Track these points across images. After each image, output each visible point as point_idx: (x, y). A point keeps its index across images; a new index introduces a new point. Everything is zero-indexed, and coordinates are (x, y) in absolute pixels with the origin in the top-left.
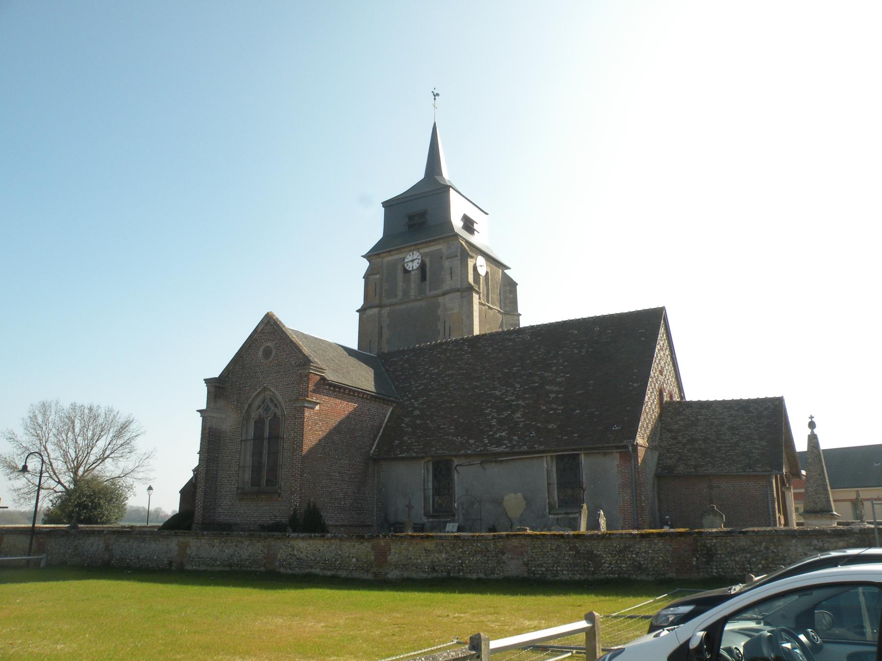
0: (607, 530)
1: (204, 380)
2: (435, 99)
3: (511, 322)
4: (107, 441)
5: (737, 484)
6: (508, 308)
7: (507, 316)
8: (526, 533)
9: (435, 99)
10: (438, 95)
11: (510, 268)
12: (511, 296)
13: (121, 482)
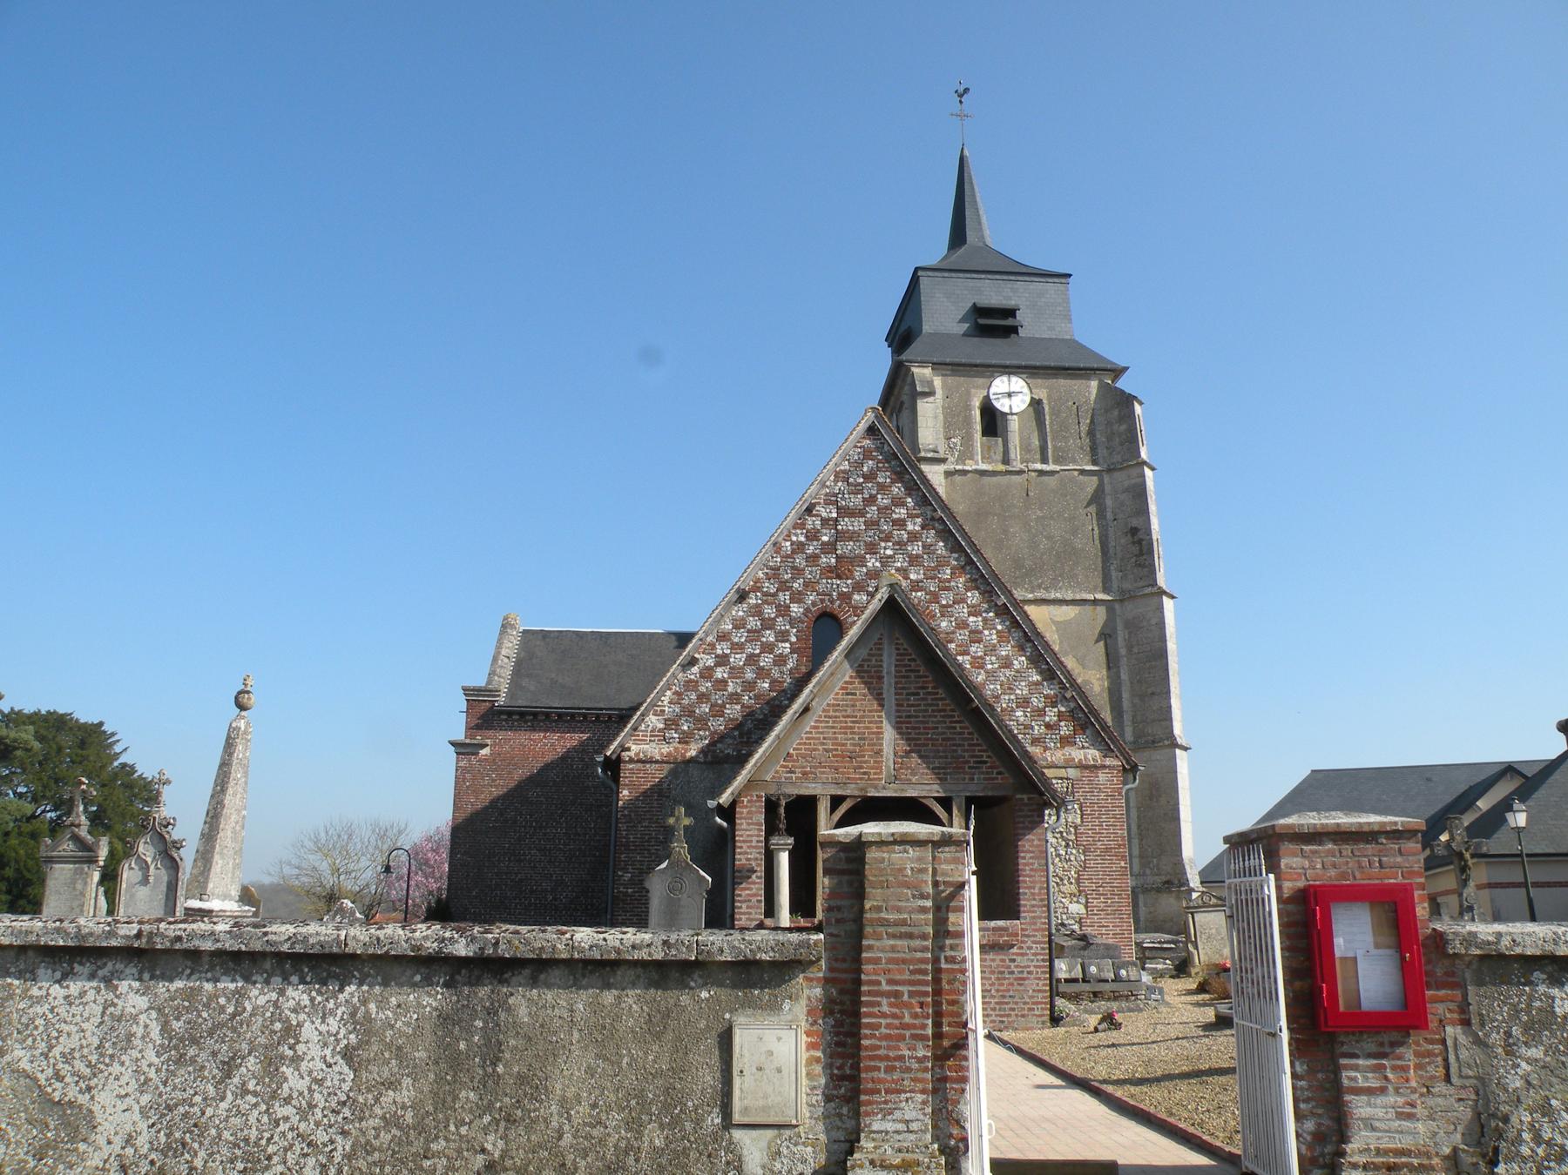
0: (1341, 958)
1: (465, 689)
2: (961, 102)
3: (1126, 484)
4: (1183, 1090)
5: (993, 960)
6: (1119, 456)
7: (1117, 475)
8: (881, 988)
9: (961, 102)
10: (966, 90)
11: (1127, 368)
12: (1123, 427)
13: (237, 898)
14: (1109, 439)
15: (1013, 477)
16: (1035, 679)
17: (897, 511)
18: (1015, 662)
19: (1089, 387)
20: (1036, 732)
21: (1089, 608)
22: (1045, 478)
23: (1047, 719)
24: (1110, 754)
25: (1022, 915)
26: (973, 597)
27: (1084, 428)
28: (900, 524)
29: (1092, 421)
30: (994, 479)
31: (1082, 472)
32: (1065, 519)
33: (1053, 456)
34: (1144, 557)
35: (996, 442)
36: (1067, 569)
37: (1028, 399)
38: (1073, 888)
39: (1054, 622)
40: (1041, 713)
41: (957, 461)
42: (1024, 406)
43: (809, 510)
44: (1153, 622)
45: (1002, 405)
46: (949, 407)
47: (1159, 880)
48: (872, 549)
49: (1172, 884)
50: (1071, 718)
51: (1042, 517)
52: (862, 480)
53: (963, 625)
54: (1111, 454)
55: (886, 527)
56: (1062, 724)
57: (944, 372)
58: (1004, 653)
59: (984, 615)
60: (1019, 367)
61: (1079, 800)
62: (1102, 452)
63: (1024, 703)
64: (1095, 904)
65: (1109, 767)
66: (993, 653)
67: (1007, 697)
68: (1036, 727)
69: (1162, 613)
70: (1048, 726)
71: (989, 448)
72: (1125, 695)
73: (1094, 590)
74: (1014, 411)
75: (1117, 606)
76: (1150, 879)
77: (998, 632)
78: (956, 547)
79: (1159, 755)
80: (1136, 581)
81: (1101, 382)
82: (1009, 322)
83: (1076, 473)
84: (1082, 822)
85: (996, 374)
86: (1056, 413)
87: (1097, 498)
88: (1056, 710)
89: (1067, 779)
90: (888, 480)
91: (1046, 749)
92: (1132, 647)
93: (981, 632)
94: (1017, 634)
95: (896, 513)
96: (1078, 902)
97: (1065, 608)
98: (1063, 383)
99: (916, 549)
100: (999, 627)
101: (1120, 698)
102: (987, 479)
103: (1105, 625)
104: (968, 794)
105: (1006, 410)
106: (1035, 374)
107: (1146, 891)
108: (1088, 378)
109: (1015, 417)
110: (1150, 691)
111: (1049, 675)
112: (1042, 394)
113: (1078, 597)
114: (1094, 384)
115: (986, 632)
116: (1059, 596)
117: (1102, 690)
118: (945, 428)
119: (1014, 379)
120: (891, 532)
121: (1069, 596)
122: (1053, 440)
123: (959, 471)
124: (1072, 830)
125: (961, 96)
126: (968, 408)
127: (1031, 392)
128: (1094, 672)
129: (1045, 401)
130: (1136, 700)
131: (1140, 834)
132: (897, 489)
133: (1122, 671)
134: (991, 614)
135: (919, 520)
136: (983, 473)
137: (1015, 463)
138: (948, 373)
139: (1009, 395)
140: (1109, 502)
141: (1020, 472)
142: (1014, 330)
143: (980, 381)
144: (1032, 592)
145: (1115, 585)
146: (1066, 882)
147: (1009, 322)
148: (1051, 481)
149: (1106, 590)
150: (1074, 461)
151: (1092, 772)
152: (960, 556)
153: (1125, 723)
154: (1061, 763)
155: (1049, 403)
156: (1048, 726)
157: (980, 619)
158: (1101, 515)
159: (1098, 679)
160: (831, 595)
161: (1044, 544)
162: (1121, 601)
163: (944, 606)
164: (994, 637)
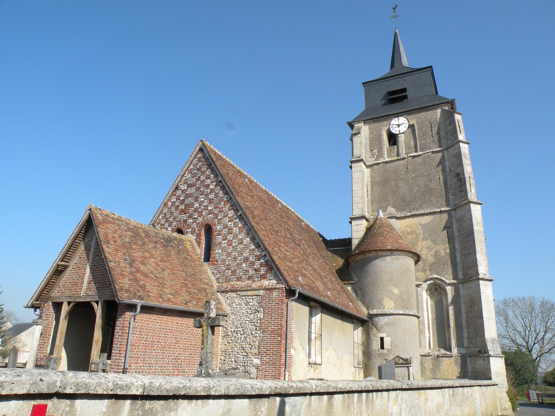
3: (454, 153)
9: (395, 11)
14: (447, 134)
15: (400, 161)
16: (252, 248)
17: (207, 181)
18: (245, 241)
19: (436, 113)
20: (250, 273)
21: (438, 216)
22: (415, 159)
23: (255, 267)
24: (280, 282)
25: (112, 357)
26: (231, 213)
27: (434, 132)
28: (207, 186)
29: (439, 128)
30: (392, 164)
31: (433, 152)
32: (426, 176)
33: (420, 148)
34: (463, 186)
35: (394, 148)
36: (427, 198)
37: (407, 126)
38: (256, 351)
39: (420, 224)
40: (253, 263)
41: (375, 160)
42: (405, 129)
43: (177, 188)
44: (468, 217)
45: (396, 131)
46: (372, 137)
47: (477, 350)
48: (196, 199)
49: (482, 352)
50: (266, 265)
51: (415, 177)
52: (196, 171)
53: (226, 226)
54: (447, 141)
55: (202, 189)
56: (262, 268)
57: (369, 123)
58: (240, 237)
59: (234, 221)
60: (402, 112)
61: (263, 306)
62: (443, 141)
63: (246, 260)
64: (264, 359)
65: (278, 288)
66: (236, 238)
67: (240, 258)
68: (250, 271)
69: (471, 212)
70: (256, 270)
71: (391, 151)
72: (458, 256)
73: (441, 206)
74: (401, 132)
75: (453, 213)
76: (473, 350)
77: (239, 228)
78: (226, 193)
79: (472, 284)
80: (460, 199)
81: (442, 109)
82: (404, 94)
83: (430, 154)
84: (264, 317)
85: (393, 118)
86: (420, 128)
87: (442, 162)
88: (259, 262)
89: (260, 296)
90: (205, 169)
91: (254, 281)
92: (460, 231)
93: (233, 229)
94: (246, 228)
95: (206, 182)
96: (258, 358)
97: (426, 217)
98: (423, 114)
99: (212, 196)
100: (240, 225)
101: (456, 257)
102: (388, 165)
103: (447, 222)
104: (104, 299)
105: (397, 133)
106: (410, 113)
107: (470, 356)
108: (436, 109)
109: (403, 135)
110: (468, 252)
111: (258, 246)
112: (414, 122)
113: (432, 211)
114: (439, 111)
115: (234, 229)
116: (423, 212)
117: (446, 254)
118: (370, 146)
119: (400, 118)
120: (204, 191)
121: (428, 211)
122: (419, 141)
123: (376, 164)
124: (259, 321)
125: (395, 9)
126: (380, 136)
127: (409, 122)
128: (441, 246)
129: (415, 125)
130: (463, 258)
131: (467, 326)
132: (208, 172)
133: (456, 244)
134: (237, 220)
135: (214, 183)
136: (387, 162)
137: (402, 155)
138: (371, 123)
139: (399, 126)
140: (447, 164)
141: (404, 158)
142: (406, 97)
143: (385, 123)
144: (410, 212)
145: (451, 203)
146: (253, 348)
147: (404, 94)
148: (418, 160)
149: (447, 205)
150: (430, 148)
151: (270, 291)
152: (228, 196)
153: (459, 269)
154: (257, 288)
155: (417, 125)
156: (256, 270)
157: (233, 223)
158: (444, 170)
159: (443, 249)
160: (181, 222)
161: (416, 189)
162: (455, 209)
163: (219, 219)
164: (238, 230)
